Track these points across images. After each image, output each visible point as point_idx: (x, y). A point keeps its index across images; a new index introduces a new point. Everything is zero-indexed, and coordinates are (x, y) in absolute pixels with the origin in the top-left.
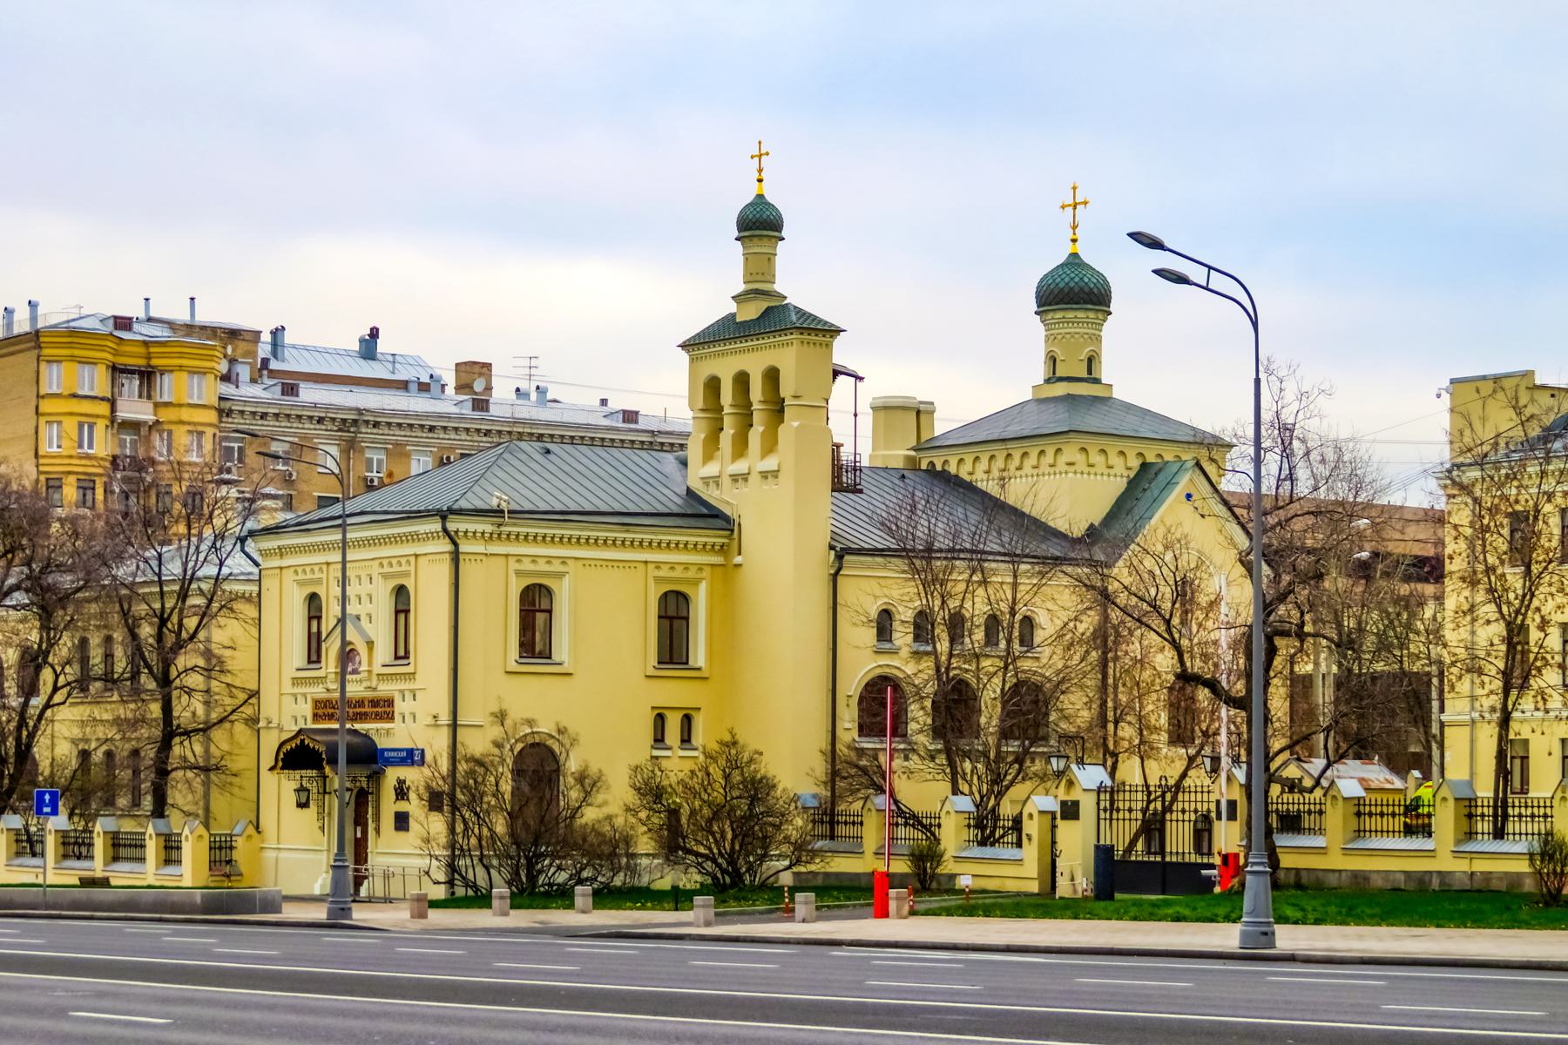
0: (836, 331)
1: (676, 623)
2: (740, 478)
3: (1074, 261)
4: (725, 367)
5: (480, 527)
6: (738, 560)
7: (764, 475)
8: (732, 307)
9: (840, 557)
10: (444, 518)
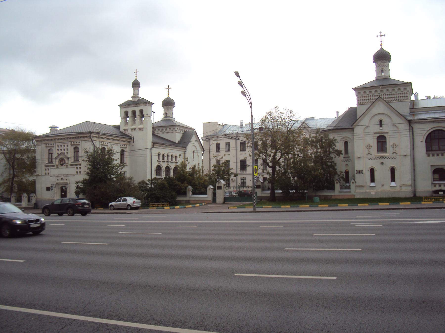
0: (152, 104)
1: (122, 155)
2: (126, 130)
3: (168, 97)
4: (130, 110)
5: (95, 135)
6: (133, 144)
7: (140, 129)
8: (131, 99)
9: (154, 144)
10: (91, 134)
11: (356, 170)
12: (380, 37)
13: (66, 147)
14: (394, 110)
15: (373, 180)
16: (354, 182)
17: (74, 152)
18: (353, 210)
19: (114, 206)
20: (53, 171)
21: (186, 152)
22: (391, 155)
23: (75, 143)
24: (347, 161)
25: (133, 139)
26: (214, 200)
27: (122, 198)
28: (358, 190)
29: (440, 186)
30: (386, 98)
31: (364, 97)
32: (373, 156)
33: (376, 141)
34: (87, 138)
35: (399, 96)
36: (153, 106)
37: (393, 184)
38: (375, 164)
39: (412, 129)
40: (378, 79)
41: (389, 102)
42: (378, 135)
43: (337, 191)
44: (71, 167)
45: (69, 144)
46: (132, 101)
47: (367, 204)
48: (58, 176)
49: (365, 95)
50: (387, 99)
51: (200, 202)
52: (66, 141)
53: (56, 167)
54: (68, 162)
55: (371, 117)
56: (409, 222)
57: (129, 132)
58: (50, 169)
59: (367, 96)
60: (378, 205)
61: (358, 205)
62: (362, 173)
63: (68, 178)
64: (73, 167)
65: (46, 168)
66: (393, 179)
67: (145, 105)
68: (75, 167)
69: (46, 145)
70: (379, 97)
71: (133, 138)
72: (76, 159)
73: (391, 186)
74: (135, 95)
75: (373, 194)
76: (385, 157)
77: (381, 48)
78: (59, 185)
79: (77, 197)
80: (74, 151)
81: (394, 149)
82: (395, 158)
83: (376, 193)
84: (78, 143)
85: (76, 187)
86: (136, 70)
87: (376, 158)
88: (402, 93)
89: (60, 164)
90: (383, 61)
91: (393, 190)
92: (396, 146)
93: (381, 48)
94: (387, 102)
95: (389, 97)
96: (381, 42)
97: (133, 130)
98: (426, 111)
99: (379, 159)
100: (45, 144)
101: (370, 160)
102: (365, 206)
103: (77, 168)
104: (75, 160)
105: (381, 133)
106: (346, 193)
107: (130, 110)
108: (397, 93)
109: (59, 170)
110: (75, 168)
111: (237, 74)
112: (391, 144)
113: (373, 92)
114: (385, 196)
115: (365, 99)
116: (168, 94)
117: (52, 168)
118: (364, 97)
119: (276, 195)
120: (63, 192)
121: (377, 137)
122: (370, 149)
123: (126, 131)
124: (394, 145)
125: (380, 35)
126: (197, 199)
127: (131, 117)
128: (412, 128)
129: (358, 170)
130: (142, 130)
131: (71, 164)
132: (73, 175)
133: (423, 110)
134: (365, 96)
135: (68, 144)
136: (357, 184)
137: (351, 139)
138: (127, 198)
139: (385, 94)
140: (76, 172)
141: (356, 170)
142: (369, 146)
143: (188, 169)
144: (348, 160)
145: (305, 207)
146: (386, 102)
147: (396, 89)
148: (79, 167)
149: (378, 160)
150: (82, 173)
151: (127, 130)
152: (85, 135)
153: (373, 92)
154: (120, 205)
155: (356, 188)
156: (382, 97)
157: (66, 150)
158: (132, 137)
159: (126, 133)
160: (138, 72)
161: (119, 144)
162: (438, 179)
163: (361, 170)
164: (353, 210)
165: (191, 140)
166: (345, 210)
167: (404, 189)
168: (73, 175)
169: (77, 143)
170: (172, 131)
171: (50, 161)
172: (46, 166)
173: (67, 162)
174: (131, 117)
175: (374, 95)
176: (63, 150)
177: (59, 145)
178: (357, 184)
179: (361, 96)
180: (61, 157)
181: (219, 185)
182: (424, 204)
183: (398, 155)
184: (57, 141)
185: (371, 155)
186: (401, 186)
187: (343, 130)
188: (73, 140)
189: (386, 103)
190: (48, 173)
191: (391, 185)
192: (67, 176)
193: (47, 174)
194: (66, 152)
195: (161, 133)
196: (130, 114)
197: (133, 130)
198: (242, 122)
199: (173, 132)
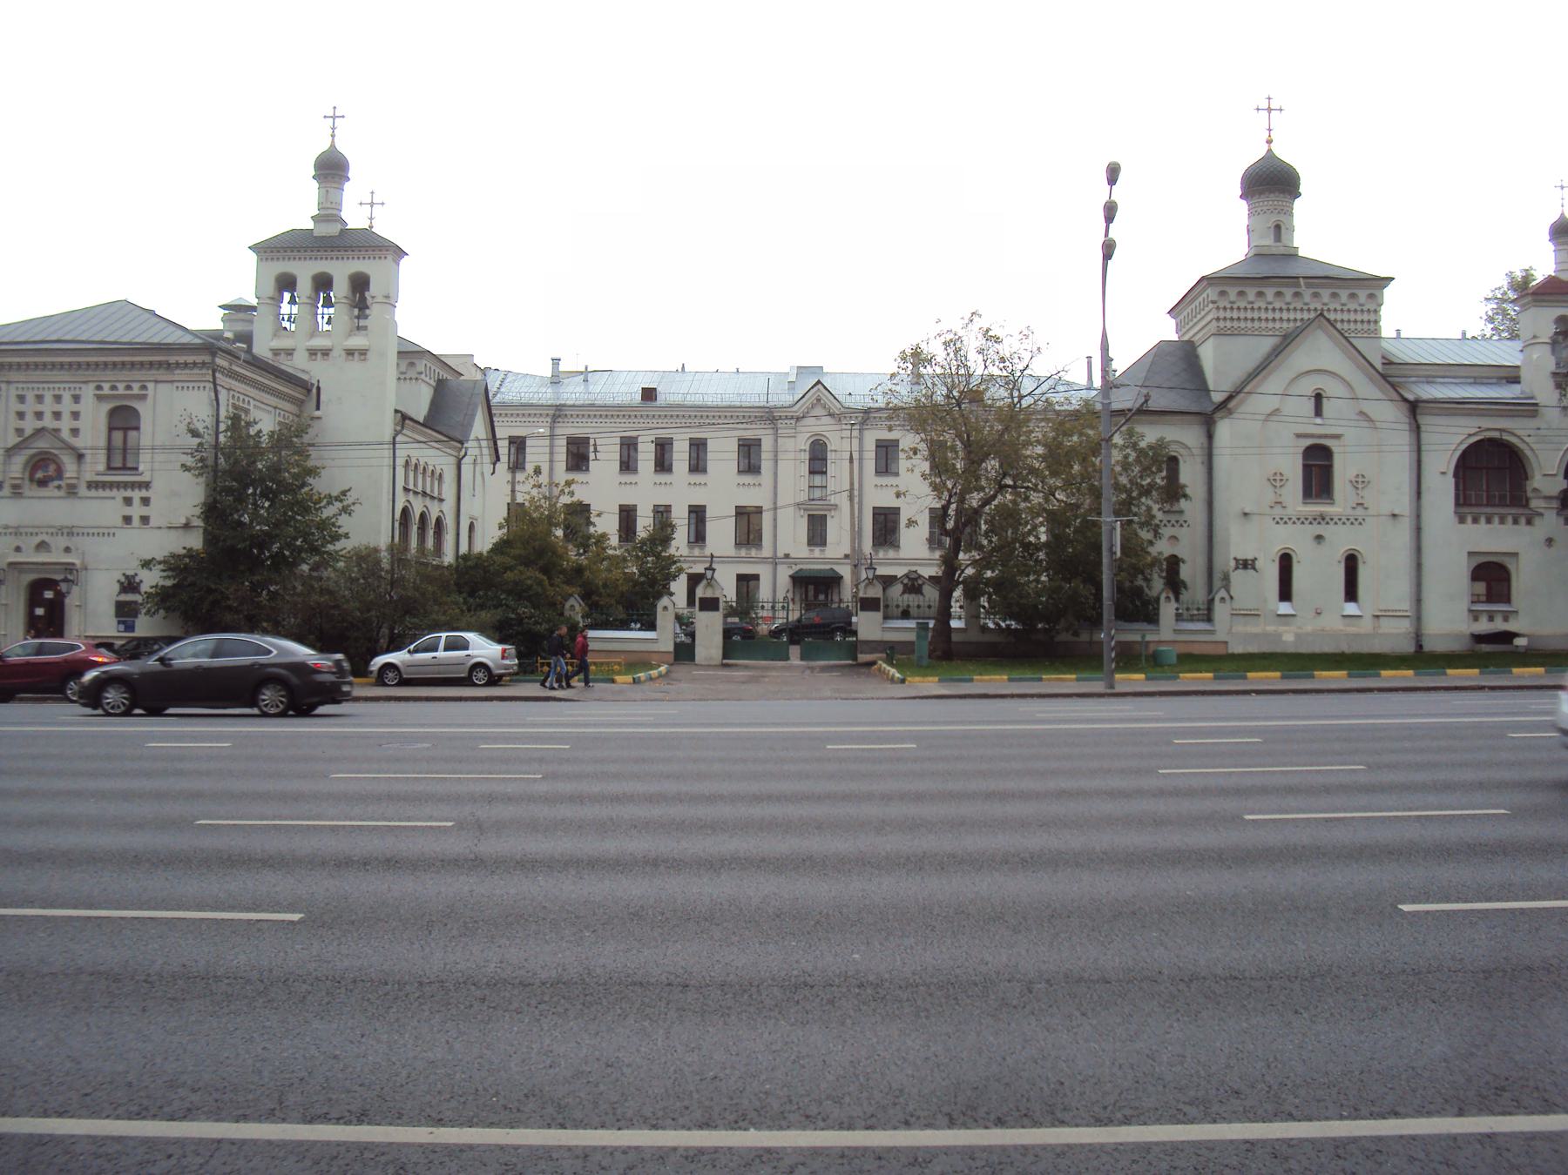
7: (350, 353)
8: (310, 225)
10: (214, 354)
11: (1235, 559)
12: (1266, 112)
13: (67, 406)
14: (1366, 364)
15: (1285, 594)
16: (1227, 597)
17: (111, 429)
18: (1370, 690)
19: (490, 664)
21: (463, 461)
22: (1349, 511)
23: (121, 390)
24: (1173, 526)
25: (314, 390)
26: (684, 652)
27: (444, 635)
28: (1241, 627)
29: (1491, 619)
30: (1342, 321)
31: (1295, 309)
32: (1290, 511)
33: (1298, 462)
34: (187, 371)
35: (1352, 319)
36: (404, 262)
37: (1351, 609)
38: (1297, 540)
39: (1417, 429)
40: (1258, 256)
41: (1353, 335)
42: (1309, 442)
43: (1168, 630)
44: (93, 493)
45: (88, 392)
46: (316, 234)
47: (1411, 672)
48: (17, 531)
49: (1242, 305)
50: (1346, 326)
51: (637, 662)
54: (79, 472)
55: (1287, 381)
57: (299, 364)
59: (1249, 306)
60: (1445, 674)
61: (1379, 675)
62: (1254, 568)
63: (73, 542)
64: (107, 493)
66: (1351, 594)
67: (284, 259)
68: (120, 494)
69: (99, 388)
70: (1321, 314)
71: (318, 389)
72: (121, 458)
73: (1344, 616)
74: (330, 212)
75: (1288, 639)
76: (1327, 519)
77: (1270, 150)
78: (21, 572)
79: (122, 627)
80: (109, 423)
81: (1359, 492)
82: (1360, 524)
83: (1298, 636)
84: (136, 390)
85: (121, 584)
86: (335, 108)
87: (1299, 519)
88: (1252, 309)
90: (1272, 195)
91: (1352, 630)
92: (1366, 483)
93: (1270, 150)
94: (1347, 335)
95: (1235, 316)
96: (1270, 130)
97: (316, 354)
98: (1475, 378)
99: (1311, 523)
101: (1281, 527)
102: (1404, 677)
103: (128, 501)
104: (113, 465)
105: (1320, 436)
106: (1196, 635)
107: (305, 272)
108: (1345, 308)
109: (23, 503)
110: (119, 500)
111: (1113, 174)
112: (1351, 473)
113: (1288, 297)
114: (1328, 648)
115: (1270, 317)
118: (1239, 308)
119: (955, 638)
120: (40, 606)
121: (1303, 449)
122: (1281, 486)
123: (283, 356)
124: (1360, 480)
125: (1272, 107)
126: (635, 647)
127: (308, 301)
128: (1418, 427)
129: (1239, 557)
130: (362, 357)
132: (105, 533)
133: (1421, 373)
134: (1299, 307)
135: (77, 392)
136: (1236, 605)
137: (1193, 450)
138: (470, 636)
139: (1306, 307)
140: (121, 519)
141: (1235, 559)
142: (1278, 478)
144: (1177, 522)
145: (1068, 681)
146: (1342, 334)
147: (1344, 295)
148: (136, 495)
149: (1307, 526)
150: (153, 523)
151: (290, 352)
152: (182, 359)
153: (1233, 296)
154: (437, 663)
155: (1234, 617)
156: (1332, 316)
157: (66, 416)
158: (312, 385)
159: (283, 367)
161: (275, 408)
162: (1484, 598)
163: (1250, 557)
164: (1370, 690)
165: (1239, 411)
166: (1204, 693)
167: (1388, 626)
169: (129, 387)
170: (405, 373)
171: (118, 463)
173: (70, 468)
174: (308, 301)
175: (1270, 307)
176: (48, 417)
177: (61, 392)
178: (1236, 605)
179: (1228, 306)
180: (42, 444)
181: (709, 594)
182: (1520, 677)
183: (1370, 512)
185: (1366, 509)
186: (1378, 616)
187: (1168, 418)
188: (110, 375)
189: (1344, 341)
191: (1345, 614)
192: (71, 534)
193: (136, 521)
194: (65, 425)
196: (340, 289)
197: (316, 354)
198: (556, 361)
199: (405, 379)
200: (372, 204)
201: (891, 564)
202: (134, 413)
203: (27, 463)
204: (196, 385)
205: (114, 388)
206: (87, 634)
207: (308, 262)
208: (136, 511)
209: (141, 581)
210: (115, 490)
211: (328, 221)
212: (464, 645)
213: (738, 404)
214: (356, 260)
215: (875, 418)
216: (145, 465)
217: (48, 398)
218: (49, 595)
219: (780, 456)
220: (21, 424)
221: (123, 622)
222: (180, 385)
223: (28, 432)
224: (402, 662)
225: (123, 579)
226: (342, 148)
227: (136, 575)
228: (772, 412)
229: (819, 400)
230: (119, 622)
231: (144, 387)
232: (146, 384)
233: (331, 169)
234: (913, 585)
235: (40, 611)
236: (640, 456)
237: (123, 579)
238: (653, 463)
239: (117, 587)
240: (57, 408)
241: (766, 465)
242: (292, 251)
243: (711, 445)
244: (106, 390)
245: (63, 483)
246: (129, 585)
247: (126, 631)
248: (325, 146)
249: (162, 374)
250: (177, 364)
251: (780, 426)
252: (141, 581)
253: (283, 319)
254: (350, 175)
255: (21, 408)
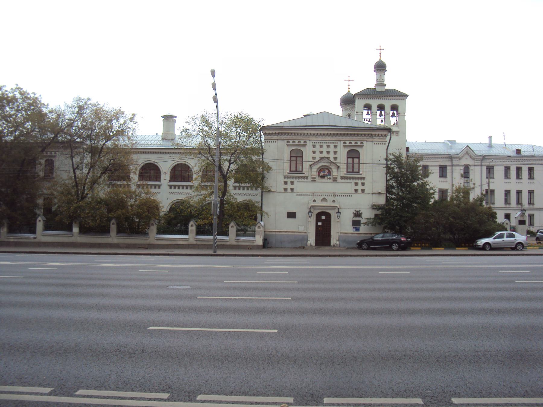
0: (406, 96)
13: (332, 149)
17: (348, 158)
19: (492, 244)
20: (301, 186)
36: (407, 100)
44: (343, 181)
48: (314, 195)
52: (332, 139)
53: (310, 179)
56: (404, 271)
58: (295, 183)
63: (336, 198)
64: (349, 181)
65: (286, 180)
67: (396, 99)
69: (288, 142)
79: (355, 230)
89: (319, 176)
100: (286, 141)
103: (356, 184)
110: (353, 184)
111: (213, 73)
116: (349, 89)
117: (300, 180)
120: (320, 222)
130: (397, 134)
131: (288, 176)
132: (349, 195)
135: (336, 144)
140: (283, 189)
143: (473, 196)
148: (360, 182)
150: (366, 192)
152: (377, 133)
160: (380, 46)
168: (349, 195)
171: (293, 169)
172: (285, 177)
184: (311, 138)
188: (349, 138)
190: (292, 190)
193: (360, 191)
194: (332, 156)
195: (333, 143)
200: (349, 81)
201: (531, 210)
202: (358, 152)
203: (318, 169)
204: (382, 143)
205: (294, 142)
206: (341, 232)
207: (376, 100)
208: (360, 187)
209: (362, 213)
210: (351, 180)
211: (381, 86)
212: (513, 236)
213: (499, 154)
214: (397, 100)
215: (425, 157)
216: (364, 171)
217: (325, 146)
218: (323, 218)
219: (454, 172)
220: (314, 155)
221: (355, 228)
222: (376, 142)
223: (317, 159)
224: (492, 242)
225: (355, 212)
226: (383, 60)
227: (360, 210)
228: (451, 156)
229: (467, 152)
230: (353, 228)
231: (362, 143)
232: (306, 141)
233: (380, 67)
234: (358, 213)
235: (320, 224)
236: (511, 172)
237: (355, 212)
238: (527, 174)
239: (353, 215)
240: (328, 150)
241: (449, 175)
242: (368, 96)
243: (535, 169)
244: (291, 143)
245: (331, 177)
246: (358, 214)
247: (356, 231)
248: (378, 60)
249: (368, 138)
250: (375, 135)
251: (453, 161)
252: (362, 213)
253: (365, 120)
254: (387, 69)
255: (314, 149)
